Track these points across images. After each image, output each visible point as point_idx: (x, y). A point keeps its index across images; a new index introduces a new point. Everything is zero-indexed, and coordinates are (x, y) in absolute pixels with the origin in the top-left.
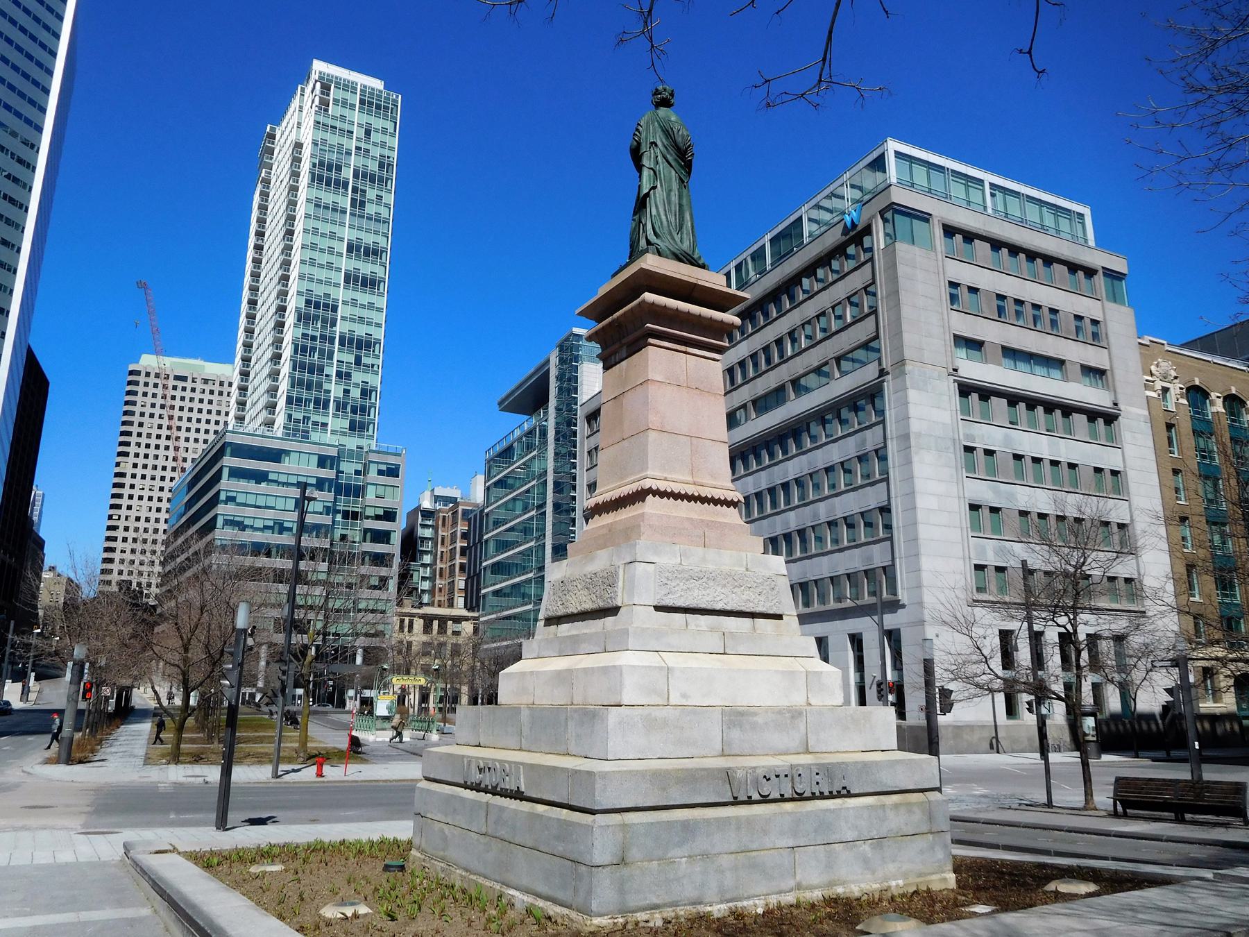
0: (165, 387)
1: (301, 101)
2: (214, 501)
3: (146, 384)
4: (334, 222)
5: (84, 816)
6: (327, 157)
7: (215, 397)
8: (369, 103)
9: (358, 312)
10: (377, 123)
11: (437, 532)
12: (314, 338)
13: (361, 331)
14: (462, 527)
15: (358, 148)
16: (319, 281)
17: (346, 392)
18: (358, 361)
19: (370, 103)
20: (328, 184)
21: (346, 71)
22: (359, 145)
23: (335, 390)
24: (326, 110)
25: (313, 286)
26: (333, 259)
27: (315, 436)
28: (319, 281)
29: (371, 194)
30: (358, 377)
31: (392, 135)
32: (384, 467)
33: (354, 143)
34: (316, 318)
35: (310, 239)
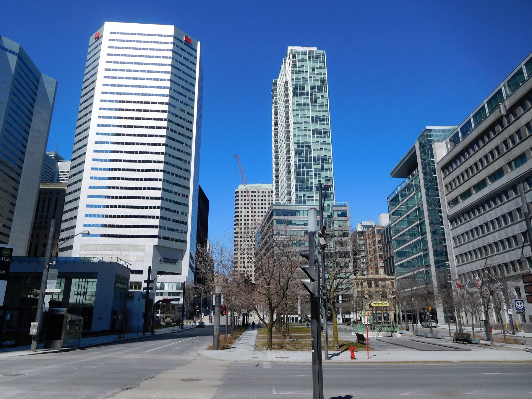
0: (248, 196)
1: (285, 65)
2: (272, 235)
3: (242, 196)
4: (305, 110)
5: (216, 389)
6: (299, 84)
7: (267, 198)
8: (313, 58)
9: (320, 146)
10: (317, 65)
11: (366, 242)
12: (303, 161)
13: (322, 154)
14: (377, 238)
15: (310, 77)
16: (302, 136)
17: (319, 181)
18: (323, 167)
19: (313, 57)
20: (300, 95)
21: (301, 47)
22: (311, 76)
23: (315, 182)
24: (296, 65)
25: (300, 139)
26: (307, 126)
27: (309, 203)
28: (302, 136)
29: (319, 95)
30: (323, 174)
31: (324, 68)
32: (340, 213)
33: (309, 76)
34: (303, 152)
35: (296, 119)
